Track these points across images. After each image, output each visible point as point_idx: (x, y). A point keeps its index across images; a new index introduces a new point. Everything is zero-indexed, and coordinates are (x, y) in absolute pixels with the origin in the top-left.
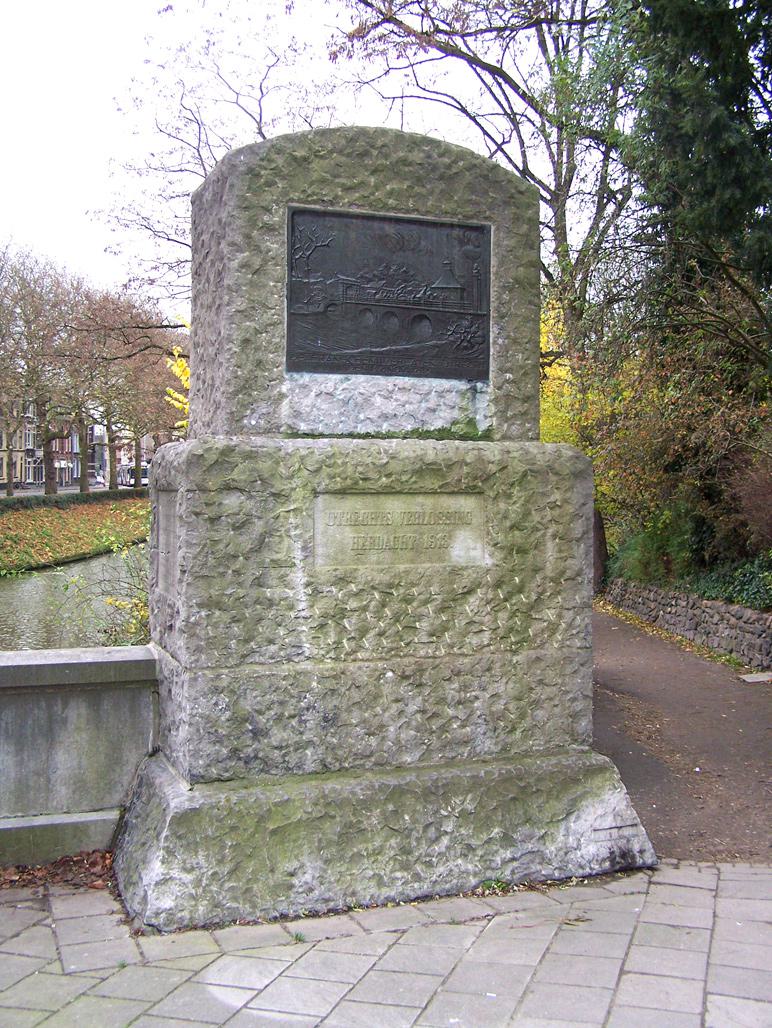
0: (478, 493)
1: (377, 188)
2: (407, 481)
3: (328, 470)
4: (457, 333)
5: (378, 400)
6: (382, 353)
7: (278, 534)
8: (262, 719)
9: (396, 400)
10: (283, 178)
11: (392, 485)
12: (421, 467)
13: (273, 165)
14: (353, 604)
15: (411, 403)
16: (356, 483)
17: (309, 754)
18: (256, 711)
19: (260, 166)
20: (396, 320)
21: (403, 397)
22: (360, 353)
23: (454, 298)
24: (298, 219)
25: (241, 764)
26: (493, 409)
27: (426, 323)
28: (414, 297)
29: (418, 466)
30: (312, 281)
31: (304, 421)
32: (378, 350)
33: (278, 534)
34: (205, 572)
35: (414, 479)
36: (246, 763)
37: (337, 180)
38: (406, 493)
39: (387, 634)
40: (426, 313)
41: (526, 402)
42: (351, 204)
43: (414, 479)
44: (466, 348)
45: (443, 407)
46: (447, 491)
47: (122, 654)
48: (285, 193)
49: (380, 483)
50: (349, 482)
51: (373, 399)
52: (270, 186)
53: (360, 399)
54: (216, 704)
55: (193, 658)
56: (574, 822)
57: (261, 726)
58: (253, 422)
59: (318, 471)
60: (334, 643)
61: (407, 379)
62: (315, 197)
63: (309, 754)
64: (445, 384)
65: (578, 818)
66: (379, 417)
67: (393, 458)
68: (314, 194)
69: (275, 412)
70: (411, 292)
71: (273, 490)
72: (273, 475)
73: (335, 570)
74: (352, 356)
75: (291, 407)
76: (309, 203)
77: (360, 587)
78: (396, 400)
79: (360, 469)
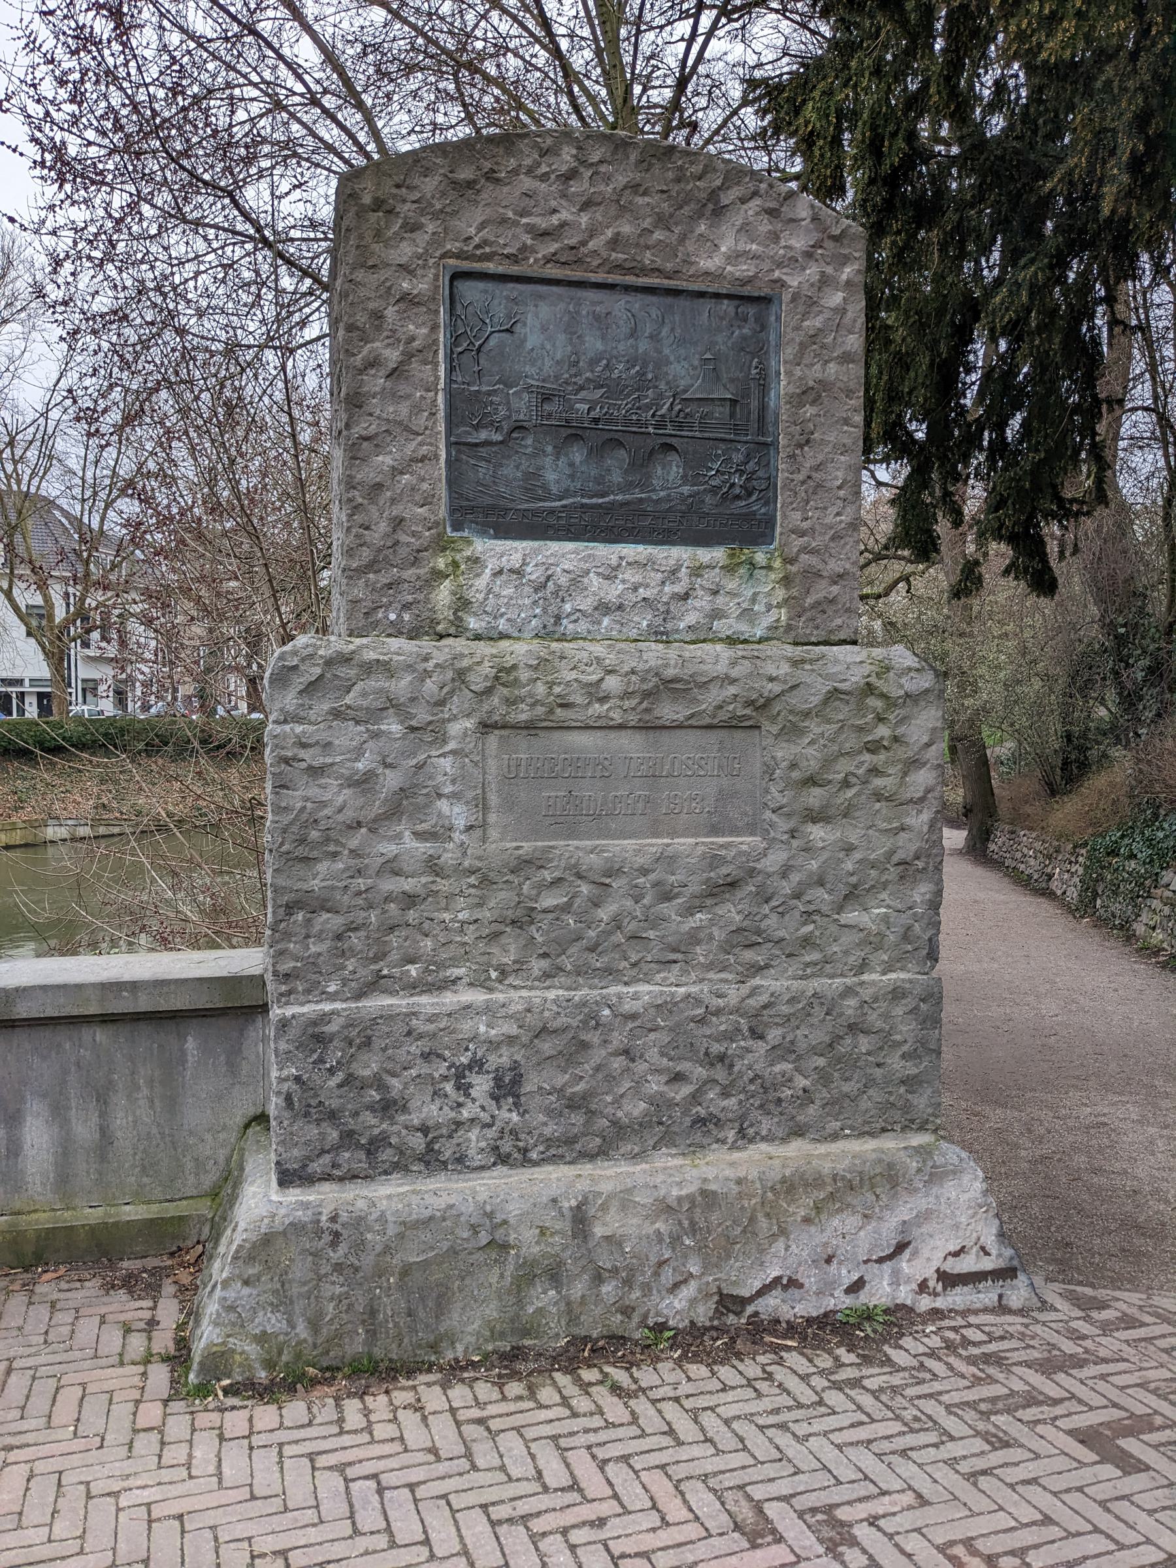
0: (751, 727)
1: (592, 233)
2: (633, 709)
3: (505, 691)
4: (723, 474)
5: (594, 581)
6: (600, 505)
7: (424, 791)
8: (395, 1083)
9: (623, 581)
10: (435, 216)
11: (611, 714)
12: (657, 686)
13: (416, 195)
14: (550, 900)
15: (647, 586)
16: (551, 712)
17: (474, 1138)
18: (388, 1072)
19: (394, 196)
20: (622, 452)
21: (632, 576)
22: (564, 506)
23: (720, 412)
24: (464, 287)
25: (362, 1155)
26: (780, 594)
27: (673, 457)
28: (653, 415)
29: (651, 684)
30: (485, 388)
31: (475, 614)
32: (594, 501)
33: (424, 791)
34: (301, 851)
35: (644, 705)
36: (369, 1153)
37: (524, 221)
38: (633, 727)
39: (600, 949)
40: (673, 441)
41: (835, 583)
42: (549, 260)
43: (644, 705)
44: (738, 497)
45: (700, 593)
46: (700, 723)
47: (222, 963)
48: (436, 240)
49: (590, 712)
50: (540, 710)
51: (586, 580)
52: (412, 231)
53: (563, 580)
54: (321, 1060)
55: (284, 988)
56: (909, 1261)
57: (394, 1094)
58: (393, 617)
59: (488, 691)
60: (515, 962)
61: (640, 548)
62: (488, 249)
63: (474, 1138)
64: (705, 555)
65: (915, 1253)
66: (596, 609)
67: (610, 672)
68: (485, 242)
69: (427, 600)
70: (648, 407)
71: (414, 723)
72: (413, 700)
73: (518, 848)
74: (552, 511)
75: (454, 593)
76: (480, 259)
77: (557, 874)
78: (623, 581)
79: (557, 690)
